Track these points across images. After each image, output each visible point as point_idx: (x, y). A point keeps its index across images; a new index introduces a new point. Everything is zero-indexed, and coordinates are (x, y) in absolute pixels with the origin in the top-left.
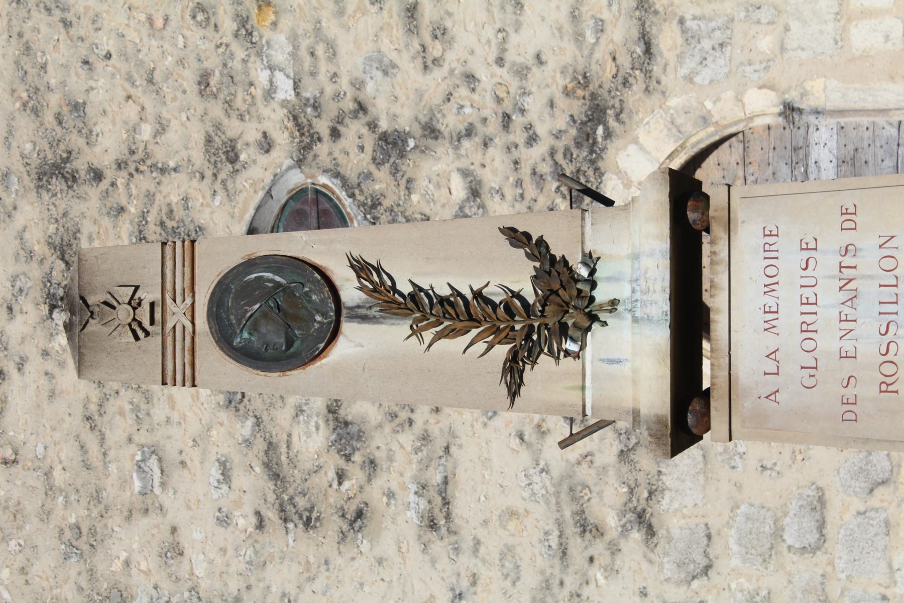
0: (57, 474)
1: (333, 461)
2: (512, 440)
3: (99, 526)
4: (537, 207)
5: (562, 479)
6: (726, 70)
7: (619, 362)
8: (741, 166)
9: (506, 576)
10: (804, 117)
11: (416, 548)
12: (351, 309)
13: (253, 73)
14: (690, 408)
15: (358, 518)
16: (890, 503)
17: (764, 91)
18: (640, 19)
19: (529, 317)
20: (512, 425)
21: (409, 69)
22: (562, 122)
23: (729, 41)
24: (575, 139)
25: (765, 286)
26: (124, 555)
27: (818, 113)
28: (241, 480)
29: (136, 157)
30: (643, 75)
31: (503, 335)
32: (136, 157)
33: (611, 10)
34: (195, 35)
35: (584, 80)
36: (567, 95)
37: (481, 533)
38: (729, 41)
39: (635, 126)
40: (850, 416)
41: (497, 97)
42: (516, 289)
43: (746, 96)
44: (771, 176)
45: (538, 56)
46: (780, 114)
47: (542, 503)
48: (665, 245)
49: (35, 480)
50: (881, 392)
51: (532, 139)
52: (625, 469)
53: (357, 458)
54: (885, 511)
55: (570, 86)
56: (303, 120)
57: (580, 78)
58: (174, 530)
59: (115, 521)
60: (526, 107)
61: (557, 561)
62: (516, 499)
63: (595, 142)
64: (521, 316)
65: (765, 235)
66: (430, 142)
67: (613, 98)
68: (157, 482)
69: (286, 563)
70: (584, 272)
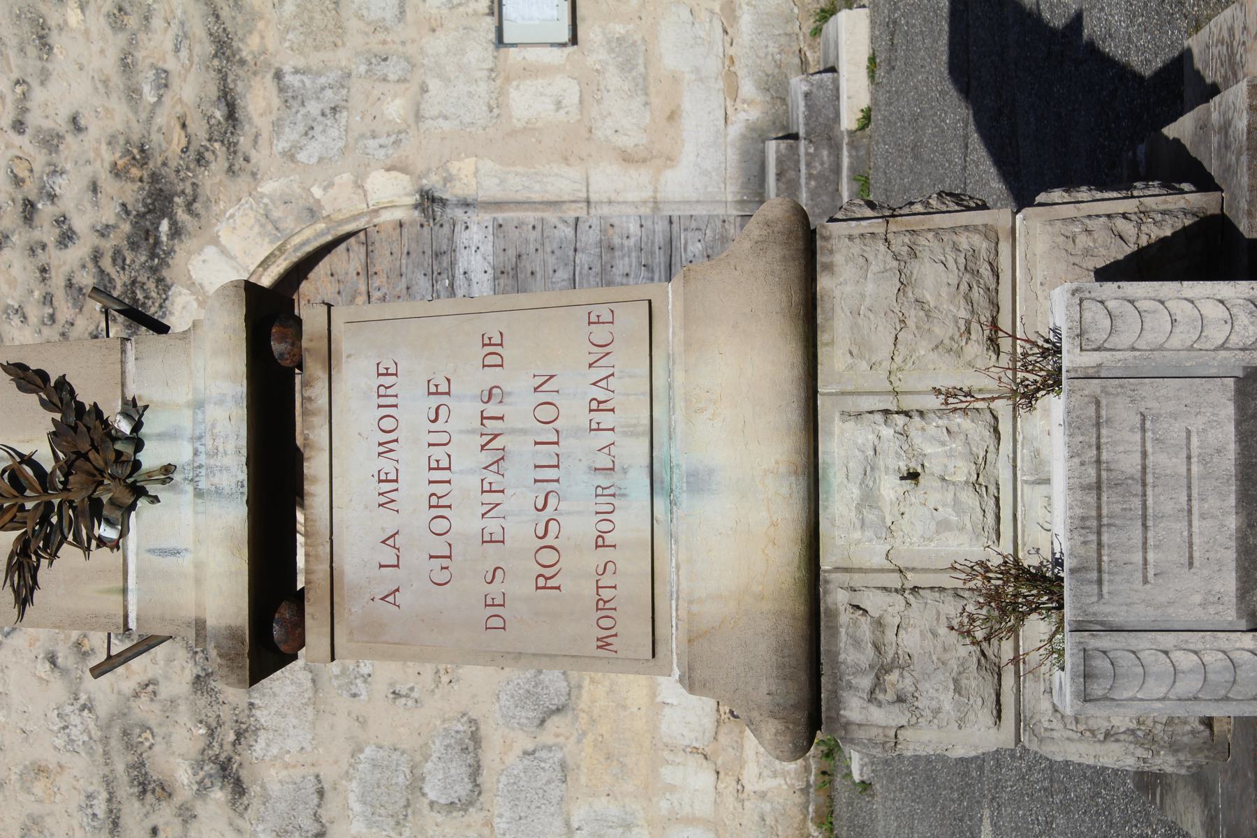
2: (39, 666)
4: (74, 333)
5: (112, 719)
6: (341, 144)
7: (175, 552)
8: (362, 279)
10: (448, 211)
14: (277, 616)
16: (567, 738)
17: (394, 174)
18: (220, 71)
19: (45, 490)
20: (38, 644)
22: (109, 214)
23: (344, 104)
24: (129, 238)
25: (380, 444)
27: (468, 205)
30: (224, 149)
31: (8, 517)
33: (178, 58)
35: (140, 154)
36: (117, 175)
38: (344, 104)
39: (214, 221)
40: (499, 623)
41: (16, 176)
42: (26, 452)
43: (369, 181)
44: (405, 291)
45: (74, 120)
46: (416, 207)
47: (83, 754)
48: (240, 388)
50: (537, 588)
51: (67, 237)
52: (202, 701)
54: (561, 748)
55: (120, 163)
57: (135, 151)
60: (58, 191)
62: (45, 750)
63: (157, 242)
64: (33, 489)
65: (379, 375)
67: (182, 180)
70: (125, 427)
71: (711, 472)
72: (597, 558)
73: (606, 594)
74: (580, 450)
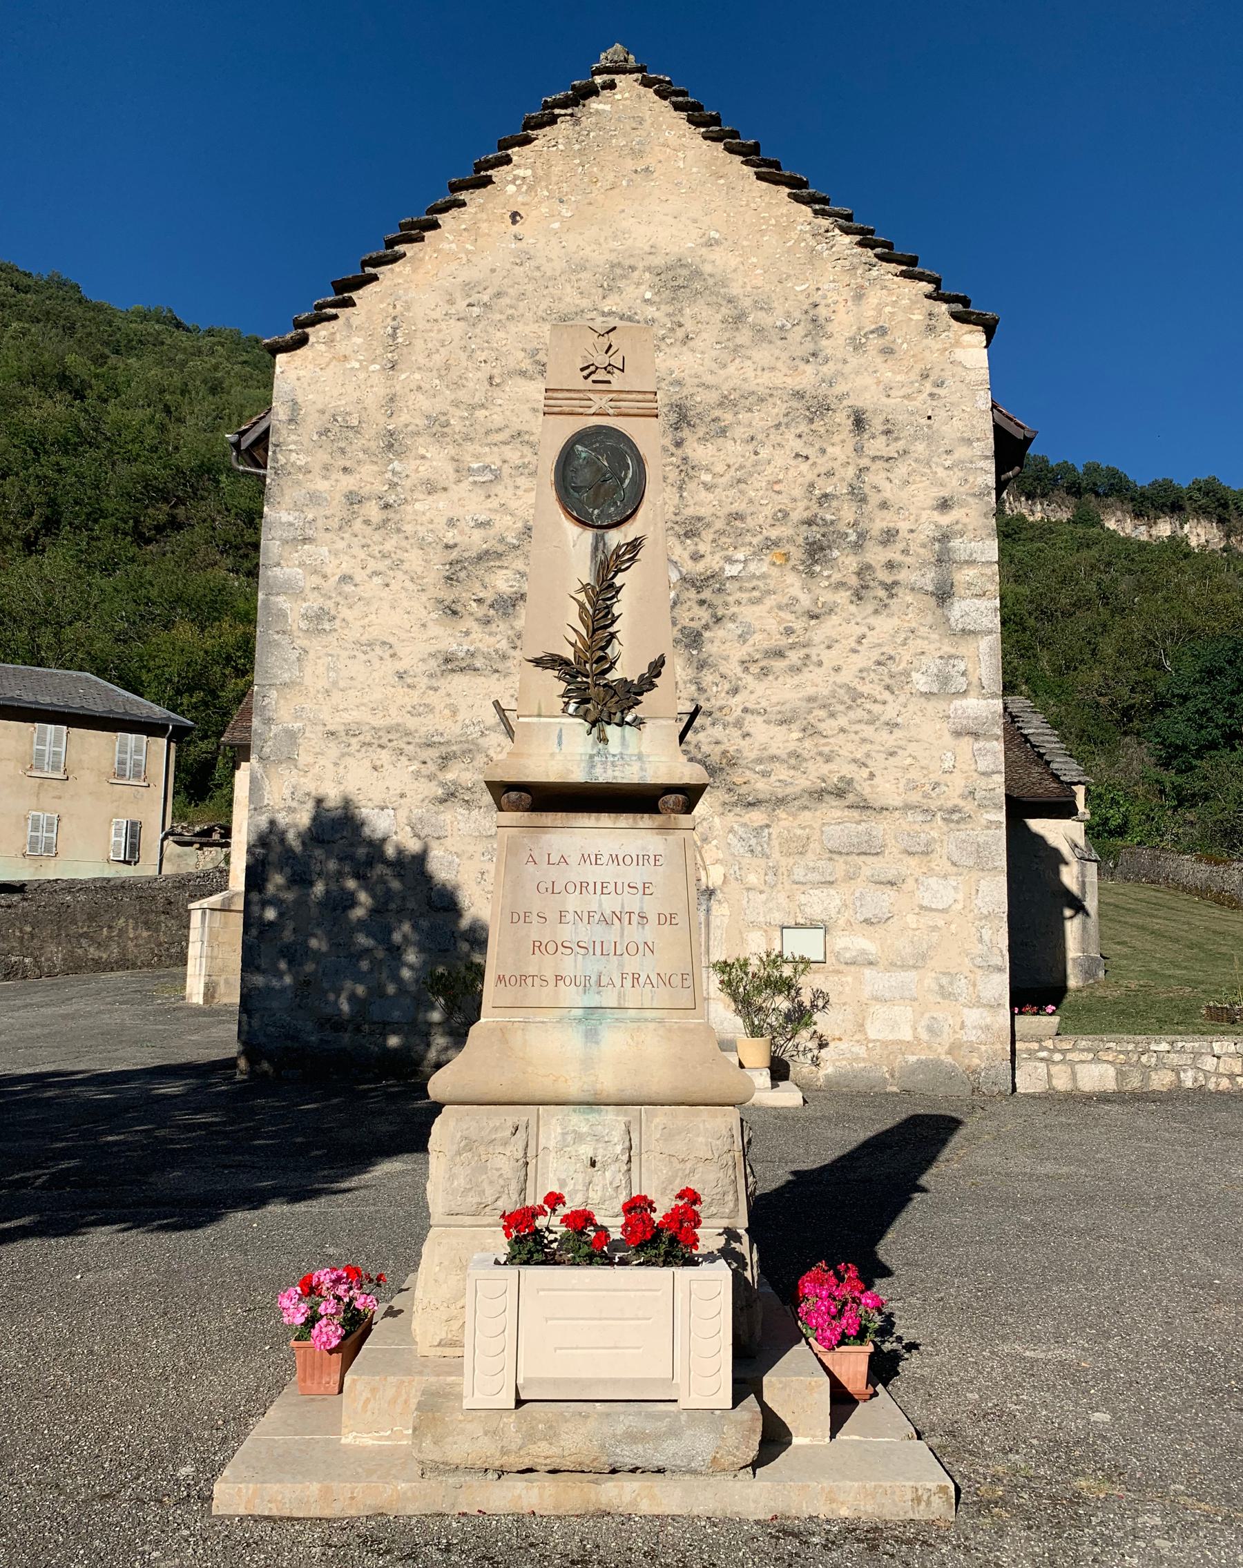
0: (484, 412)
1: (489, 595)
5: (477, 745)
7: (560, 744)
9: (414, 707)
11: (432, 650)
12: (603, 537)
15: (453, 612)
21: (739, 652)
22: (705, 749)
26: (428, 455)
28: (477, 535)
34: (768, 511)
35: (732, 763)
37: (442, 692)
49: (479, 398)
53: (492, 612)
58: (445, 489)
59: (451, 450)
61: (424, 740)
66: (695, 665)
68: (476, 479)
70: (629, 718)
71: (597, 1043)
72: (549, 975)
73: (529, 980)
74: (611, 968)
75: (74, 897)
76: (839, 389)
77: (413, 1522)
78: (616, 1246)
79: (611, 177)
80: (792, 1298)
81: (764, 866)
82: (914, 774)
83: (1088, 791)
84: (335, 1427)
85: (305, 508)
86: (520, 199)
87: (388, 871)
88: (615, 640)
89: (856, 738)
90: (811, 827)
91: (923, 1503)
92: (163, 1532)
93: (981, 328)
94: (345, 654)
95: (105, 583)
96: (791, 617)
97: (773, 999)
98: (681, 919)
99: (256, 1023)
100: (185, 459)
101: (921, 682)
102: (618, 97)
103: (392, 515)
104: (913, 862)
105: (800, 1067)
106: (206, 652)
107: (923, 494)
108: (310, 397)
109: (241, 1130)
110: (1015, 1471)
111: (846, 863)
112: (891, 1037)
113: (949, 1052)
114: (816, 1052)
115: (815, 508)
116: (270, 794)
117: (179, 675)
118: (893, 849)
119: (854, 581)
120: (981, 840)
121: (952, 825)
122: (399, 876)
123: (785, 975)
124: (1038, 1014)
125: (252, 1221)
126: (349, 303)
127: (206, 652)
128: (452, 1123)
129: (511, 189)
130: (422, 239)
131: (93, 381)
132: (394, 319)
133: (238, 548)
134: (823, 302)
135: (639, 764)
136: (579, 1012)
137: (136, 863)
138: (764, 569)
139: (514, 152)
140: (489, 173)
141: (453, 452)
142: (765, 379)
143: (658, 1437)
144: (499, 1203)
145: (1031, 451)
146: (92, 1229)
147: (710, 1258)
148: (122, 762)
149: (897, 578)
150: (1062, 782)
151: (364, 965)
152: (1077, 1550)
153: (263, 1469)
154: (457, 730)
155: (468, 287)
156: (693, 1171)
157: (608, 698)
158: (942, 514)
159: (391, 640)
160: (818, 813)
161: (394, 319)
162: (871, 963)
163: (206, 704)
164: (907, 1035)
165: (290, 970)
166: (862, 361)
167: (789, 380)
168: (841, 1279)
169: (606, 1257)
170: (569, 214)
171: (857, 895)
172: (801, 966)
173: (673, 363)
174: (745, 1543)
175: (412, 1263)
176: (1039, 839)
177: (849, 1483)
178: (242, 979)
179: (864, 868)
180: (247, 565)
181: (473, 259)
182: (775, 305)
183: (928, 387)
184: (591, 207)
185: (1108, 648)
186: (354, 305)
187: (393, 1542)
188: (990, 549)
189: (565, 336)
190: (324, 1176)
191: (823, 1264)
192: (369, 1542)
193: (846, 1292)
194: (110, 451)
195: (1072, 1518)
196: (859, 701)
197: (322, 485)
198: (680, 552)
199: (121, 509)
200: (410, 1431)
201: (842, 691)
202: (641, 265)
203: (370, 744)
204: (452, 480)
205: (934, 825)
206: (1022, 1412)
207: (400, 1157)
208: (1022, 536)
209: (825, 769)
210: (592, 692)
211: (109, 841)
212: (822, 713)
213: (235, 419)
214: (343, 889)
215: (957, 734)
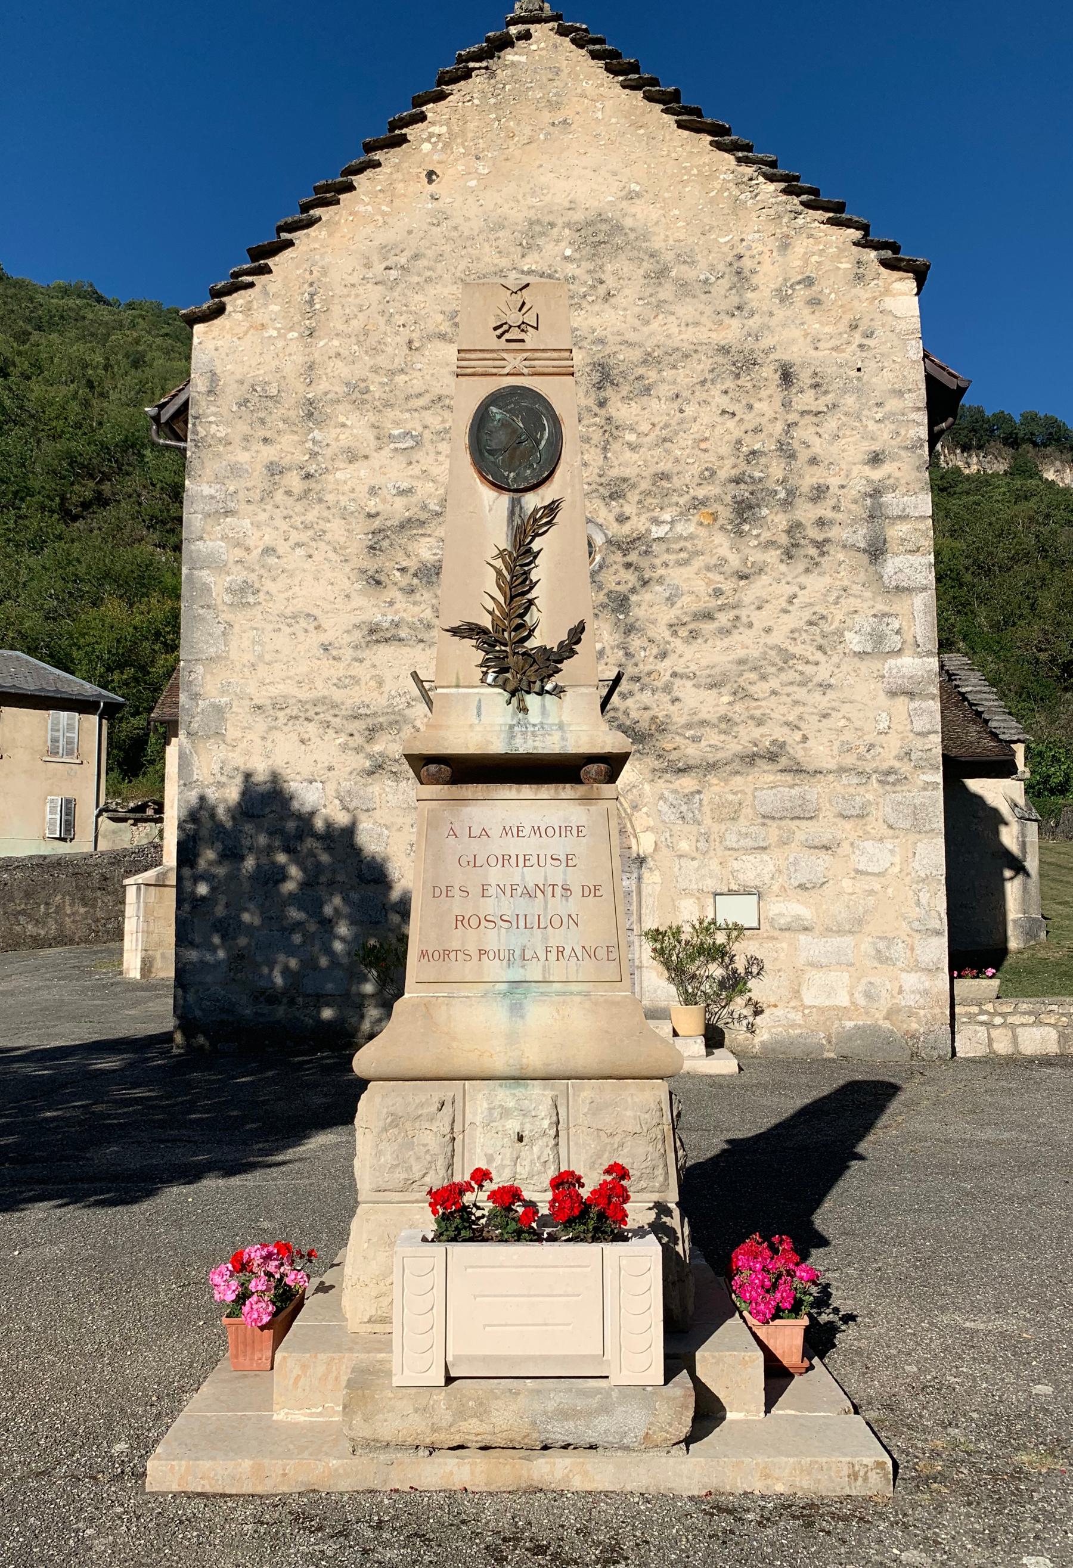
1: (412, 564)
3: (368, 406)
5: (404, 716)
7: (479, 714)
9: (339, 679)
11: (357, 622)
12: (519, 501)
13: (669, 510)
21: (667, 615)
22: (634, 715)
26: (349, 423)
28: (400, 503)
29: (614, 430)
32: (614, 430)
34: (695, 470)
35: (662, 729)
37: (367, 663)
40: (437, 894)
45: (677, 699)
49: (399, 363)
53: (415, 581)
56: (638, 543)
58: (366, 457)
59: (371, 417)
61: (350, 713)
66: (622, 629)
69: (346, 533)
70: (549, 687)
73: (453, 955)
75: (11, 874)
76: (766, 342)
77: (345, 1498)
78: (544, 1222)
79: (527, 131)
80: (726, 1270)
81: (695, 833)
82: (849, 736)
83: (1028, 749)
84: (267, 1404)
85: (226, 481)
86: (436, 157)
87: (317, 844)
88: (533, 607)
89: (789, 700)
90: (742, 792)
91: (860, 1479)
92: (97, 1509)
93: (911, 275)
94: (270, 627)
95: (33, 561)
96: (721, 578)
97: (707, 967)
98: (606, 891)
99: (191, 998)
100: (109, 435)
101: (855, 641)
102: (534, 47)
103: (313, 485)
104: (848, 825)
105: (736, 1034)
106: (135, 628)
107: (852, 450)
108: (228, 367)
109: (177, 1104)
110: (955, 1445)
111: (779, 828)
112: (827, 1003)
113: (886, 1018)
114: (751, 1019)
115: (743, 466)
116: (200, 770)
117: (109, 652)
118: (828, 812)
119: (784, 539)
120: (917, 802)
121: (888, 787)
122: (328, 849)
123: (718, 942)
124: (977, 977)
125: (187, 1196)
126: (266, 270)
127: (135, 628)
128: (378, 1100)
129: (426, 147)
130: (338, 202)
131: (17, 359)
132: (311, 284)
133: (164, 523)
134: (748, 253)
135: (560, 733)
136: (503, 987)
137: (71, 840)
138: (692, 529)
139: (429, 109)
140: (403, 131)
141: (373, 419)
142: (690, 334)
143: (590, 1414)
144: (427, 1179)
145: (965, 401)
146: (30, 1206)
147: (640, 1233)
148: (55, 740)
149: (830, 535)
150: (1001, 741)
151: (297, 939)
152: (1018, 1527)
153: (195, 1446)
154: (383, 701)
155: (385, 250)
156: (622, 1145)
157: (527, 667)
158: (874, 468)
159: (316, 612)
160: (750, 778)
161: (311, 284)
162: (806, 929)
163: (136, 680)
164: (844, 1000)
165: (223, 943)
166: (789, 313)
167: (714, 335)
168: (775, 1251)
169: (534, 1233)
170: (486, 171)
171: (791, 860)
172: (735, 933)
173: (594, 321)
174: (679, 1520)
175: (342, 1237)
176: (979, 800)
177: (785, 1459)
178: (176, 954)
179: (798, 832)
180: (173, 539)
181: (389, 220)
182: (699, 257)
183: (857, 338)
184: (508, 163)
185: (1047, 602)
186: (270, 271)
187: (325, 1519)
188: (924, 504)
189: (477, 295)
190: (259, 1150)
191: (756, 1237)
192: (300, 1519)
193: (780, 1265)
194: (35, 428)
195: (1013, 1494)
196: (791, 663)
197: (243, 457)
198: (605, 514)
199: (47, 487)
200: (340, 1408)
201: (773, 653)
202: (560, 222)
203: (297, 718)
204: (372, 447)
205: (870, 788)
206: (962, 1385)
207: (334, 1130)
208: (958, 490)
209: (756, 733)
210: (511, 661)
211: (44, 818)
212: (753, 676)
213: (158, 392)
214: (273, 863)
215: (892, 694)
